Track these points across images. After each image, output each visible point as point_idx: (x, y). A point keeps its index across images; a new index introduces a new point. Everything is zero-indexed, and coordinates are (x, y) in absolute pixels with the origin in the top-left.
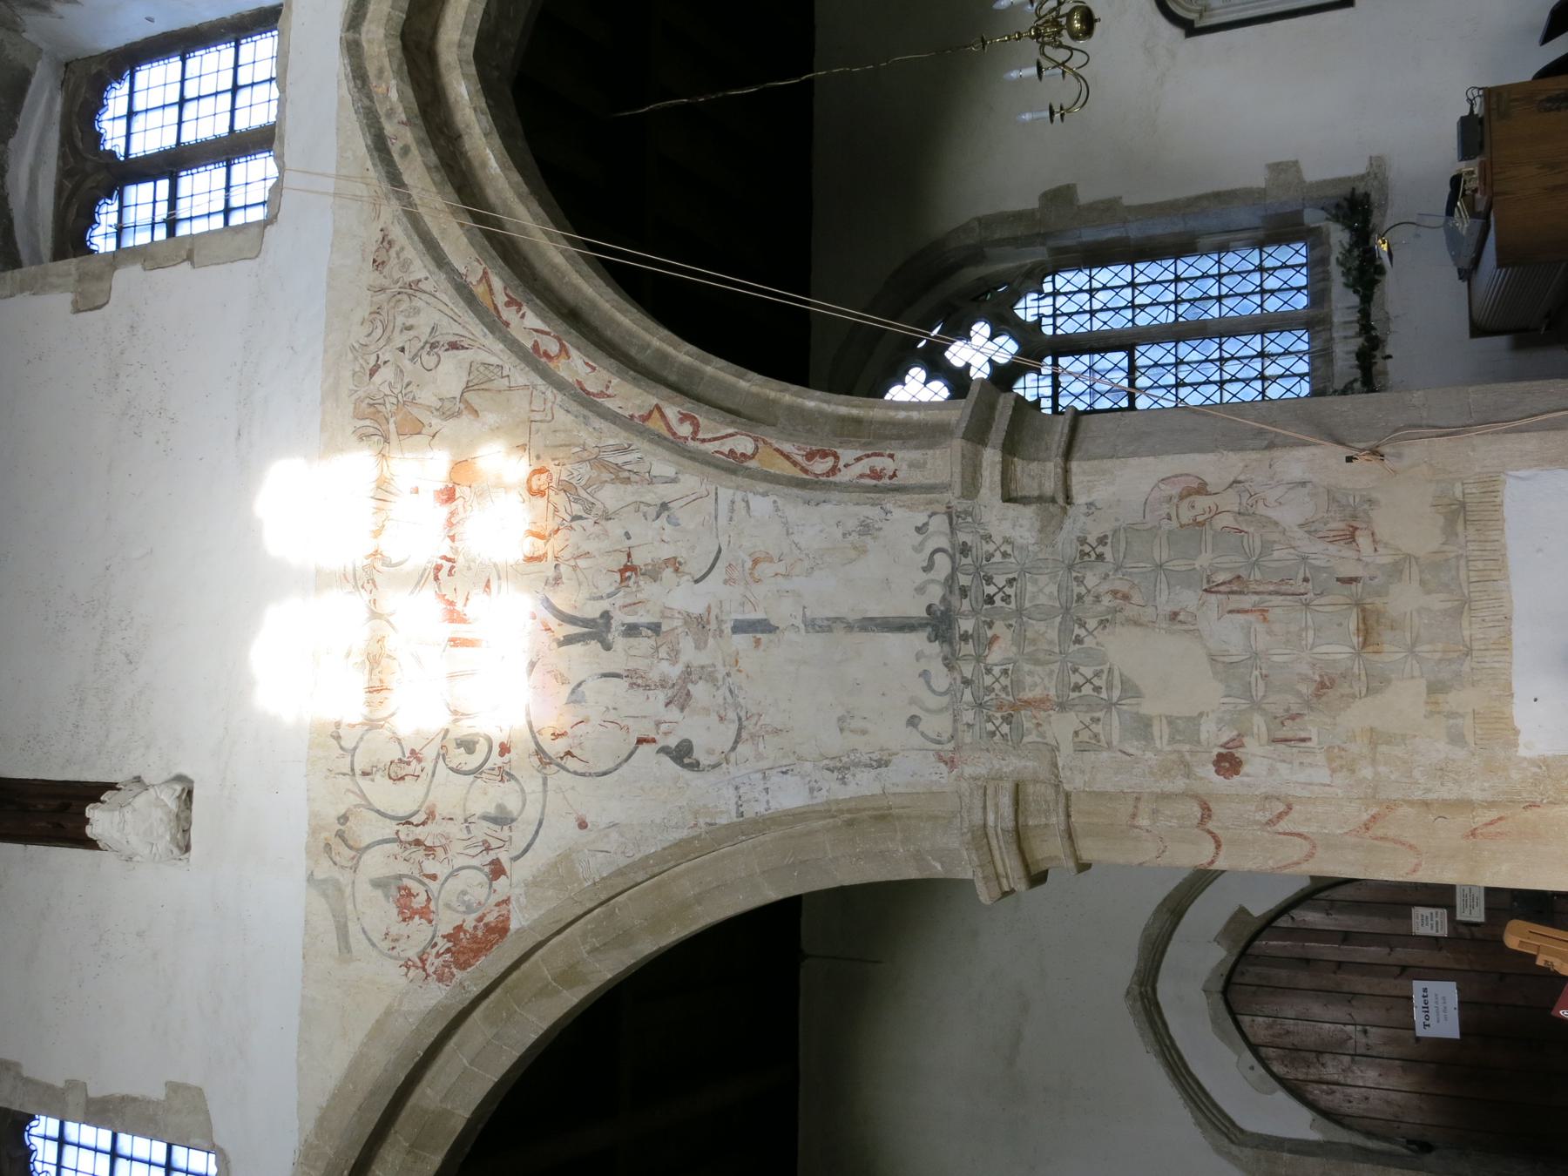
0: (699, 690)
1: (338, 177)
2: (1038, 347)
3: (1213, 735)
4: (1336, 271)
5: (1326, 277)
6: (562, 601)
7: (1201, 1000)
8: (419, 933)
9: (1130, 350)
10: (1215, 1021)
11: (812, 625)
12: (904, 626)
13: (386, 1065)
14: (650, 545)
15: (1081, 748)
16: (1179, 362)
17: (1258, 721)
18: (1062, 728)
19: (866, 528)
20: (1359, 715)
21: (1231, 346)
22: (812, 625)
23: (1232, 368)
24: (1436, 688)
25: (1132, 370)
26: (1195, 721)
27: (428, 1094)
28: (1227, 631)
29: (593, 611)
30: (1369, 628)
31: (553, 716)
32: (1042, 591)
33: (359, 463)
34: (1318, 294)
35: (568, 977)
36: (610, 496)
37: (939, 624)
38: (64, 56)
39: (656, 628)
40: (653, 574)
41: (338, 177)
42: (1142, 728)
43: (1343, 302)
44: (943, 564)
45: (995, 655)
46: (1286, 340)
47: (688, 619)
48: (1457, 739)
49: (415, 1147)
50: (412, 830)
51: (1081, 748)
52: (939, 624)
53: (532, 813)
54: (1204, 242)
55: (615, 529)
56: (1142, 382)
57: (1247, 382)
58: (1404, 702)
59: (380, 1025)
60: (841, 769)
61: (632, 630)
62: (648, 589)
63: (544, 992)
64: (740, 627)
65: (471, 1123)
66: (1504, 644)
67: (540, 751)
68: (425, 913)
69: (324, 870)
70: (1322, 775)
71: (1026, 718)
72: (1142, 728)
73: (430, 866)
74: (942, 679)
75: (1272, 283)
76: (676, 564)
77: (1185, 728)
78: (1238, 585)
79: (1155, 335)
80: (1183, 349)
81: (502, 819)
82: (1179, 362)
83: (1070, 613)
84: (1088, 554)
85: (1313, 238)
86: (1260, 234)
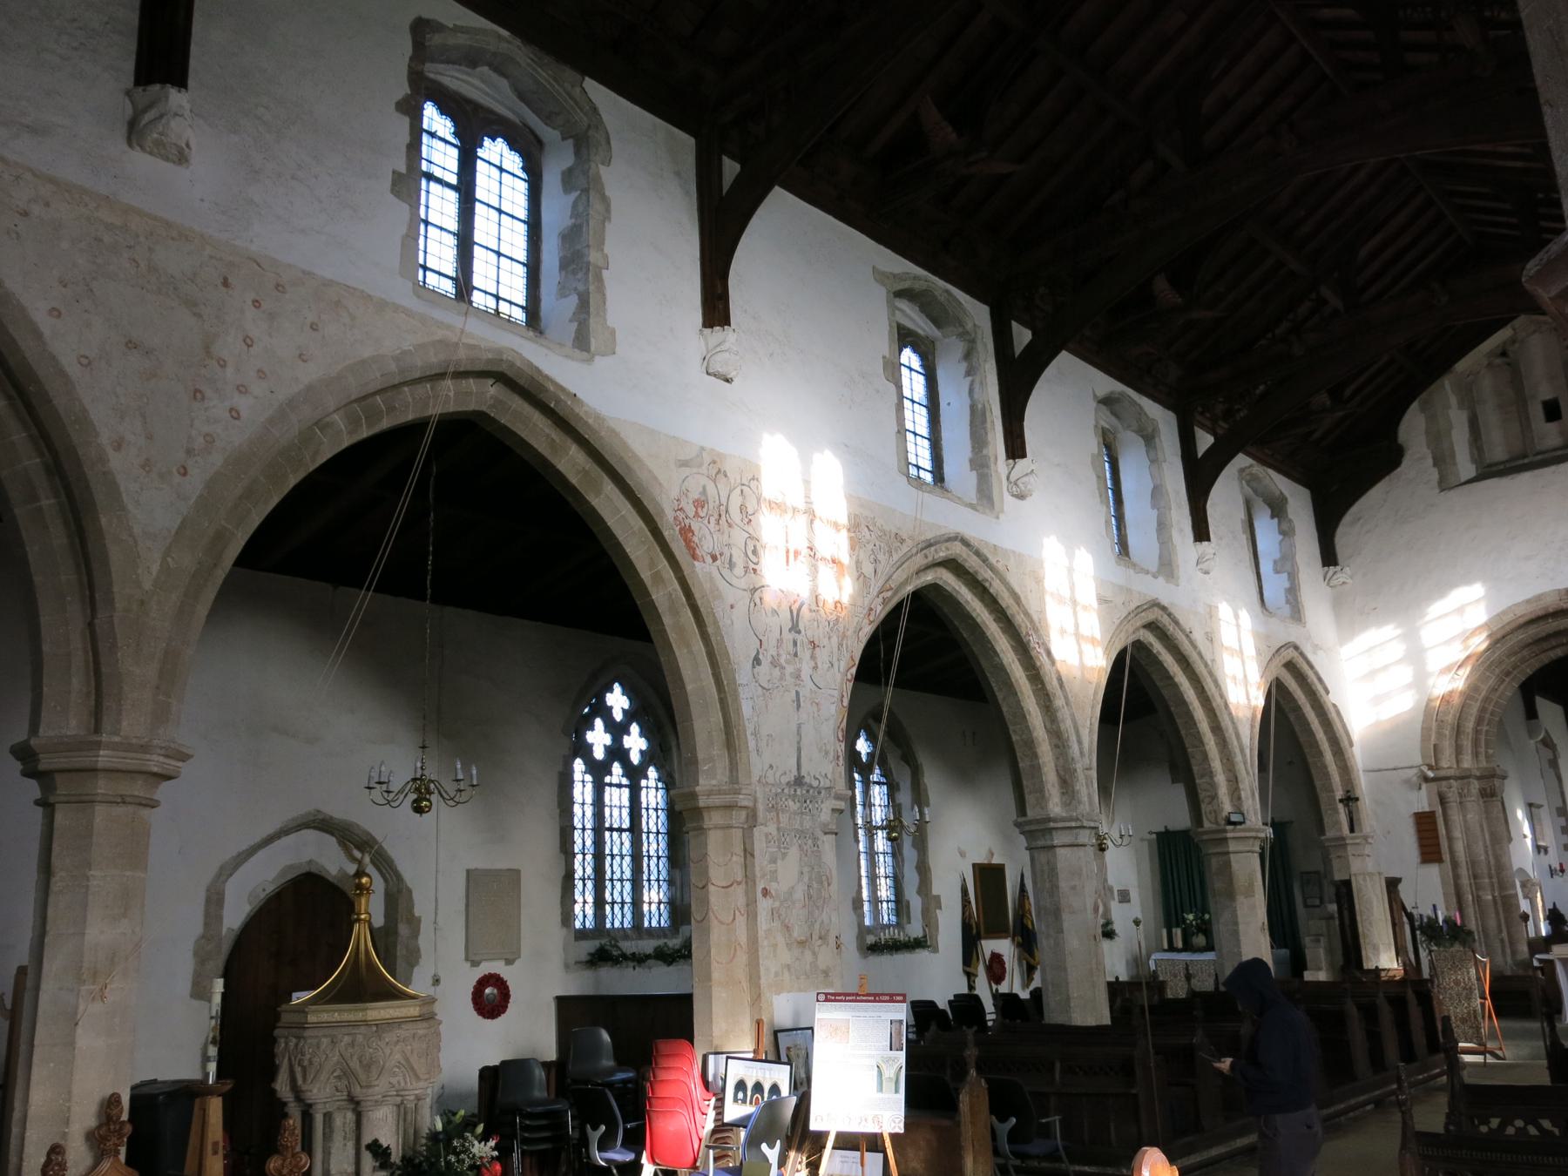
0: (777, 672)
1: (1228, 853)
2: (634, 775)
3: (773, 887)
4: (661, 942)
5: (659, 937)
6: (805, 609)
7: (305, 858)
8: (691, 510)
9: (630, 830)
10: (291, 867)
11: (799, 727)
12: (799, 768)
13: (639, 478)
14: (822, 656)
15: (767, 835)
16: (622, 857)
17: (777, 904)
18: (772, 828)
19: (827, 753)
20: (780, 940)
21: (628, 886)
22: (799, 727)
23: (618, 885)
24: (789, 967)
25: (620, 830)
26: (776, 880)
27: (609, 487)
28: (799, 894)
29: (801, 627)
30: (802, 943)
31: (770, 599)
32: (807, 824)
33: (843, 520)
34: (651, 932)
35: (657, 577)
36: (835, 640)
37: (799, 781)
38: (938, 345)
39: (796, 655)
40: (813, 657)
41: (1228, 853)
42: (773, 861)
43: (648, 946)
44: (815, 783)
45: (791, 803)
46: (629, 916)
47: (799, 670)
48: (777, 974)
49: (586, 473)
50: (722, 513)
51: (767, 835)
52: (799, 781)
53: (734, 581)
54: (677, 873)
55: (825, 641)
56: (615, 834)
57: (621, 893)
58: (785, 956)
59: (655, 478)
60: (755, 734)
61: (795, 643)
62: (808, 654)
63: (652, 564)
64: (797, 693)
65: (594, 510)
66: (800, 990)
67: (755, 590)
68: (697, 515)
69: (707, 458)
70: (764, 927)
71: (773, 814)
72: (773, 861)
73: (713, 520)
74: (784, 780)
75: (617, 908)
76: (815, 668)
77: (774, 876)
78: (810, 897)
79: (636, 844)
80: (628, 859)
81: (731, 565)
82: (622, 857)
83: (801, 833)
84: (815, 839)
85: (899, 925)
86: (678, 902)
